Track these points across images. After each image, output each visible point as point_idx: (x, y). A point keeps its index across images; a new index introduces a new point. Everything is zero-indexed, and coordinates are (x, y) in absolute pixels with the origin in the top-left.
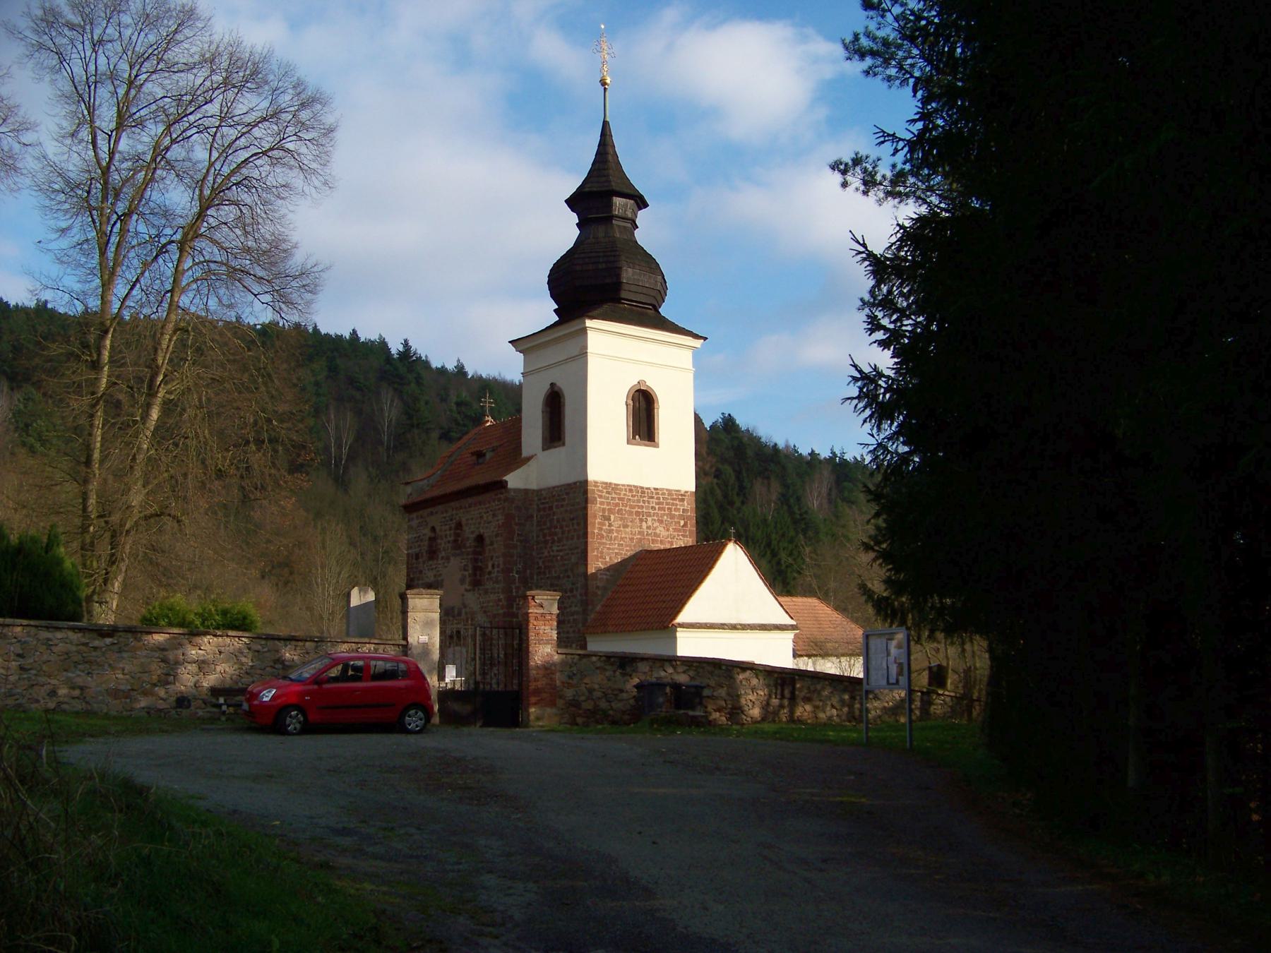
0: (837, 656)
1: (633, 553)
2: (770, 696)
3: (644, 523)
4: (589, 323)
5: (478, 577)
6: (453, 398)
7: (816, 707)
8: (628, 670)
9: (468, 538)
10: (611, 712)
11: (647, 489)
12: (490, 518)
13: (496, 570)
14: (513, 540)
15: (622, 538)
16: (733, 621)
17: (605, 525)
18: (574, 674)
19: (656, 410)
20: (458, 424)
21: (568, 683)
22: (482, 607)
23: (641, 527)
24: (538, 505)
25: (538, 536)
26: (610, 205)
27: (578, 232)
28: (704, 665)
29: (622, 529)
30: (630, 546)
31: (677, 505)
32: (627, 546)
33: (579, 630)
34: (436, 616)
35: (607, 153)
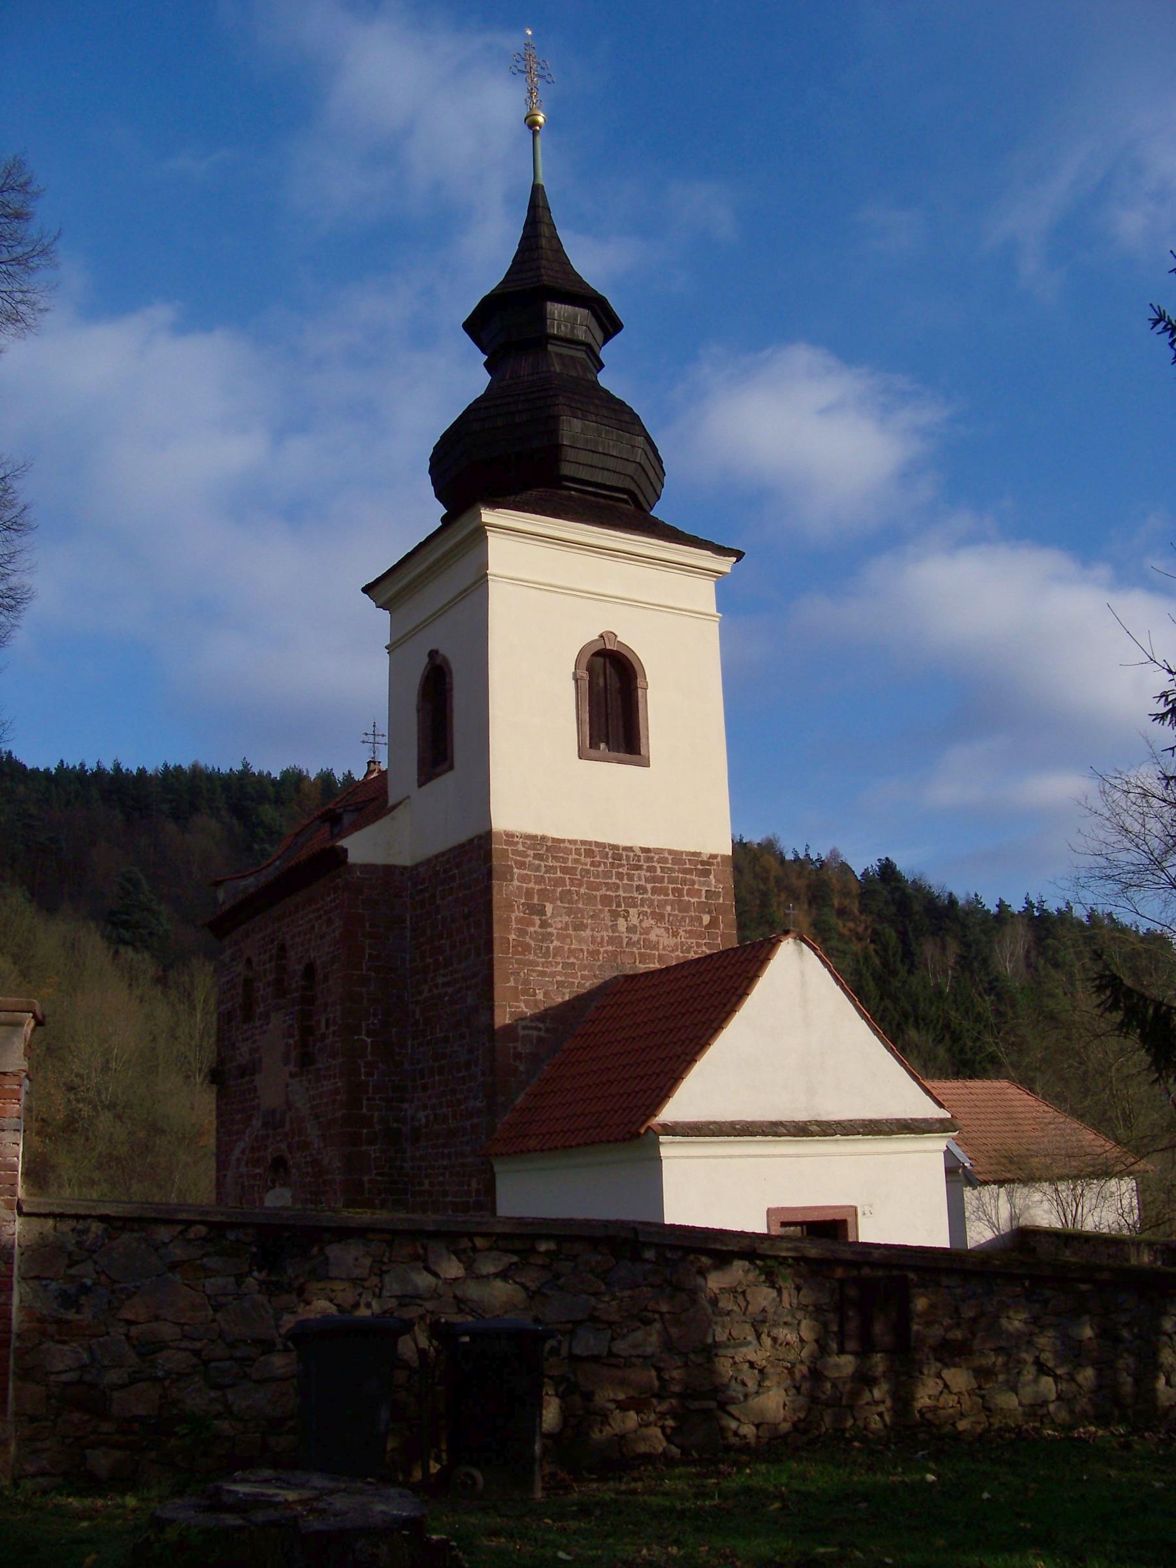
0: (1051, 1181)
1: (597, 982)
2: (822, 1348)
4: (488, 516)
7: (983, 1374)
10: (224, 1426)
11: (626, 849)
13: (332, 1029)
14: (362, 970)
15: (572, 952)
16: (802, 1116)
18: (84, 1289)
19: (640, 692)
21: (59, 1321)
23: (614, 927)
26: (541, 317)
29: (571, 932)
31: (693, 883)
32: (584, 968)
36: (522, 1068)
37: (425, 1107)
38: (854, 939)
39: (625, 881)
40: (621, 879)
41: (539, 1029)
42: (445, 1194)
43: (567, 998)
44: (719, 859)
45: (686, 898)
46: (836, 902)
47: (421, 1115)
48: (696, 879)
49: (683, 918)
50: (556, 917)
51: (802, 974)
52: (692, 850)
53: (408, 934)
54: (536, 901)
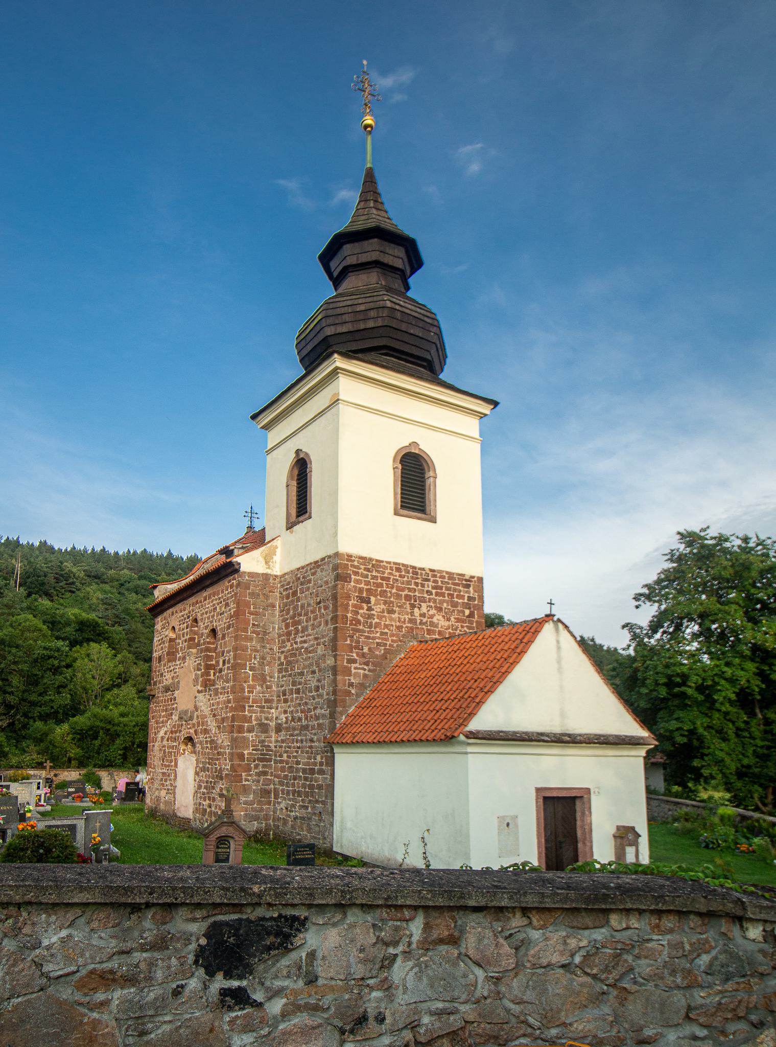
3: (416, 610)
11: (420, 569)
12: (223, 609)
13: (227, 666)
15: (386, 626)
16: (557, 729)
17: (363, 609)
22: (212, 710)
23: (412, 614)
29: (385, 614)
30: (397, 635)
31: (460, 591)
32: (392, 635)
36: (353, 692)
37: (285, 712)
39: (420, 587)
40: (417, 586)
41: (365, 670)
42: (298, 763)
44: (476, 579)
45: (456, 600)
47: (283, 716)
48: (462, 589)
49: (454, 610)
51: (558, 642)
52: (460, 573)
54: (364, 595)
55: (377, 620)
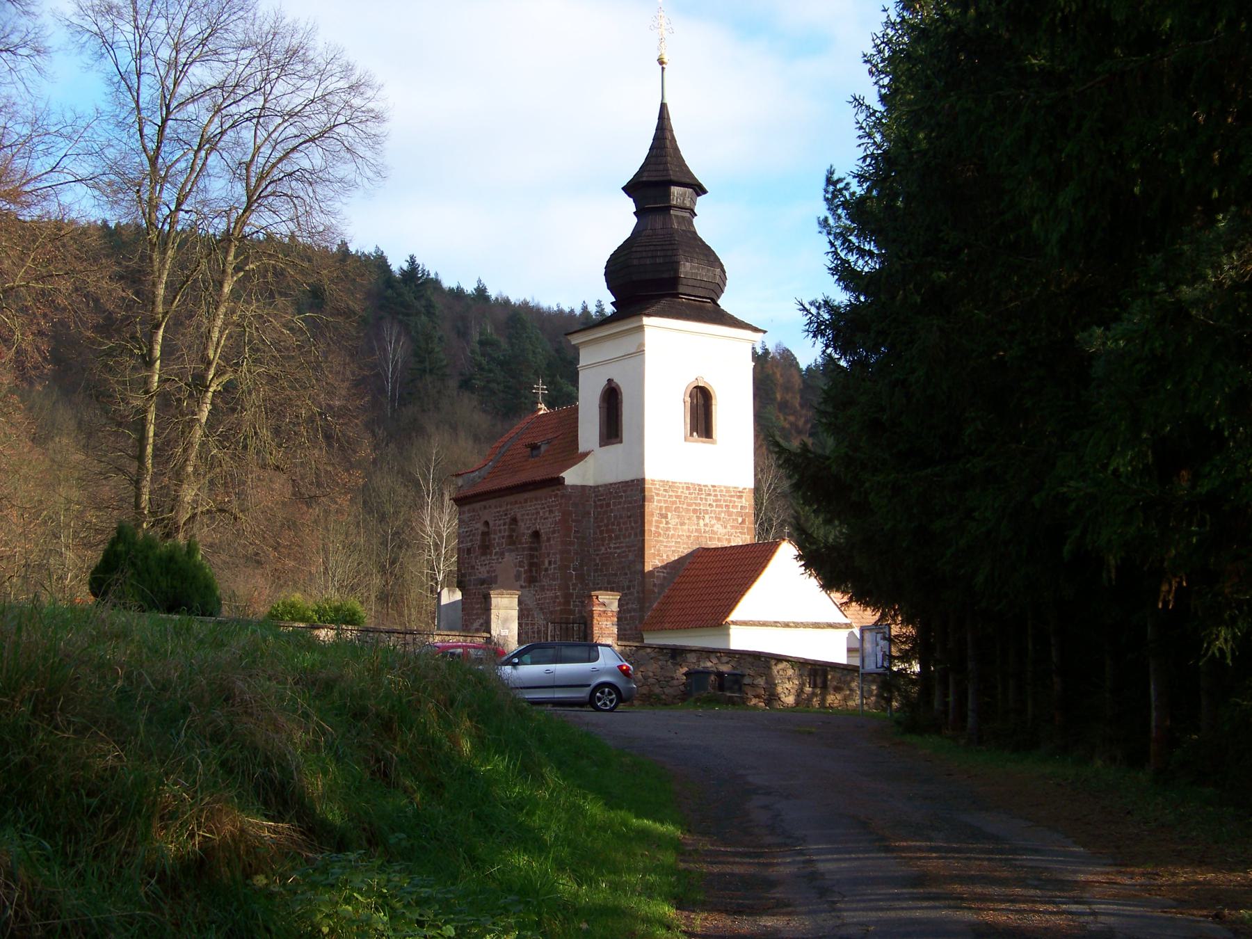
1: (690, 550)
5: (534, 574)
6: (476, 337)
8: (678, 659)
9: (524, 534)
10: (664, 697)
11: (704, 486)
12: (547, 514)
16: (786, 619)
20: (481, 368)
22: (538, 604)
23: (698, 524)
24: (595, 502)
25: (595, 533)
26: (668, 195)
27: (635, 220)
28: (746, 657)
29: (679, 527)
30: (687, 544)
31: (735, 502)
32: (684, 544)
33: (636, 627)
34: (515, 613)
35: (665, 147)
36: (656, 591)
38: (793, 432)
43: (676, 558)
46: (778, 396)
50: (673, 519)
53: (592, 520)
55: (672, 532)
